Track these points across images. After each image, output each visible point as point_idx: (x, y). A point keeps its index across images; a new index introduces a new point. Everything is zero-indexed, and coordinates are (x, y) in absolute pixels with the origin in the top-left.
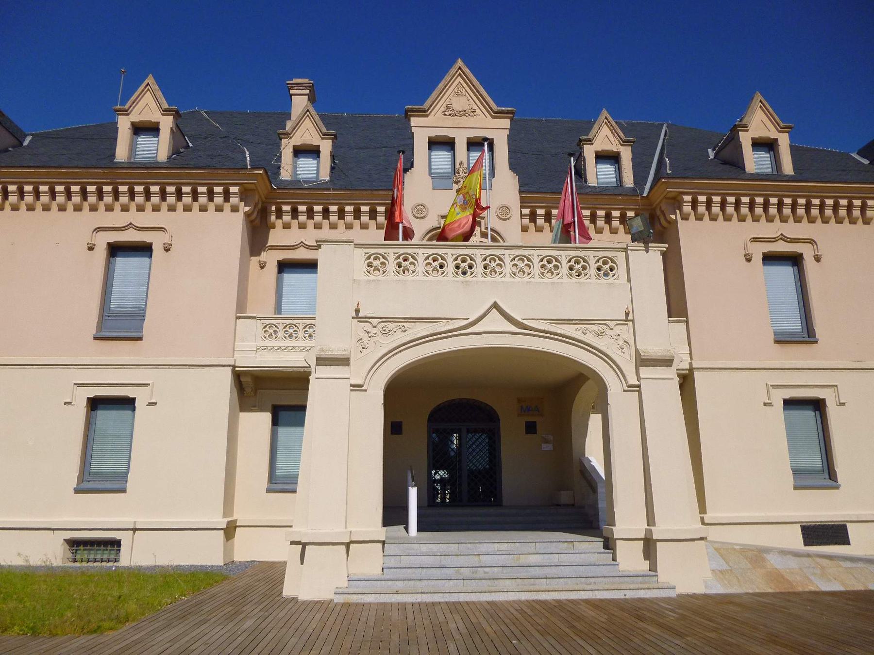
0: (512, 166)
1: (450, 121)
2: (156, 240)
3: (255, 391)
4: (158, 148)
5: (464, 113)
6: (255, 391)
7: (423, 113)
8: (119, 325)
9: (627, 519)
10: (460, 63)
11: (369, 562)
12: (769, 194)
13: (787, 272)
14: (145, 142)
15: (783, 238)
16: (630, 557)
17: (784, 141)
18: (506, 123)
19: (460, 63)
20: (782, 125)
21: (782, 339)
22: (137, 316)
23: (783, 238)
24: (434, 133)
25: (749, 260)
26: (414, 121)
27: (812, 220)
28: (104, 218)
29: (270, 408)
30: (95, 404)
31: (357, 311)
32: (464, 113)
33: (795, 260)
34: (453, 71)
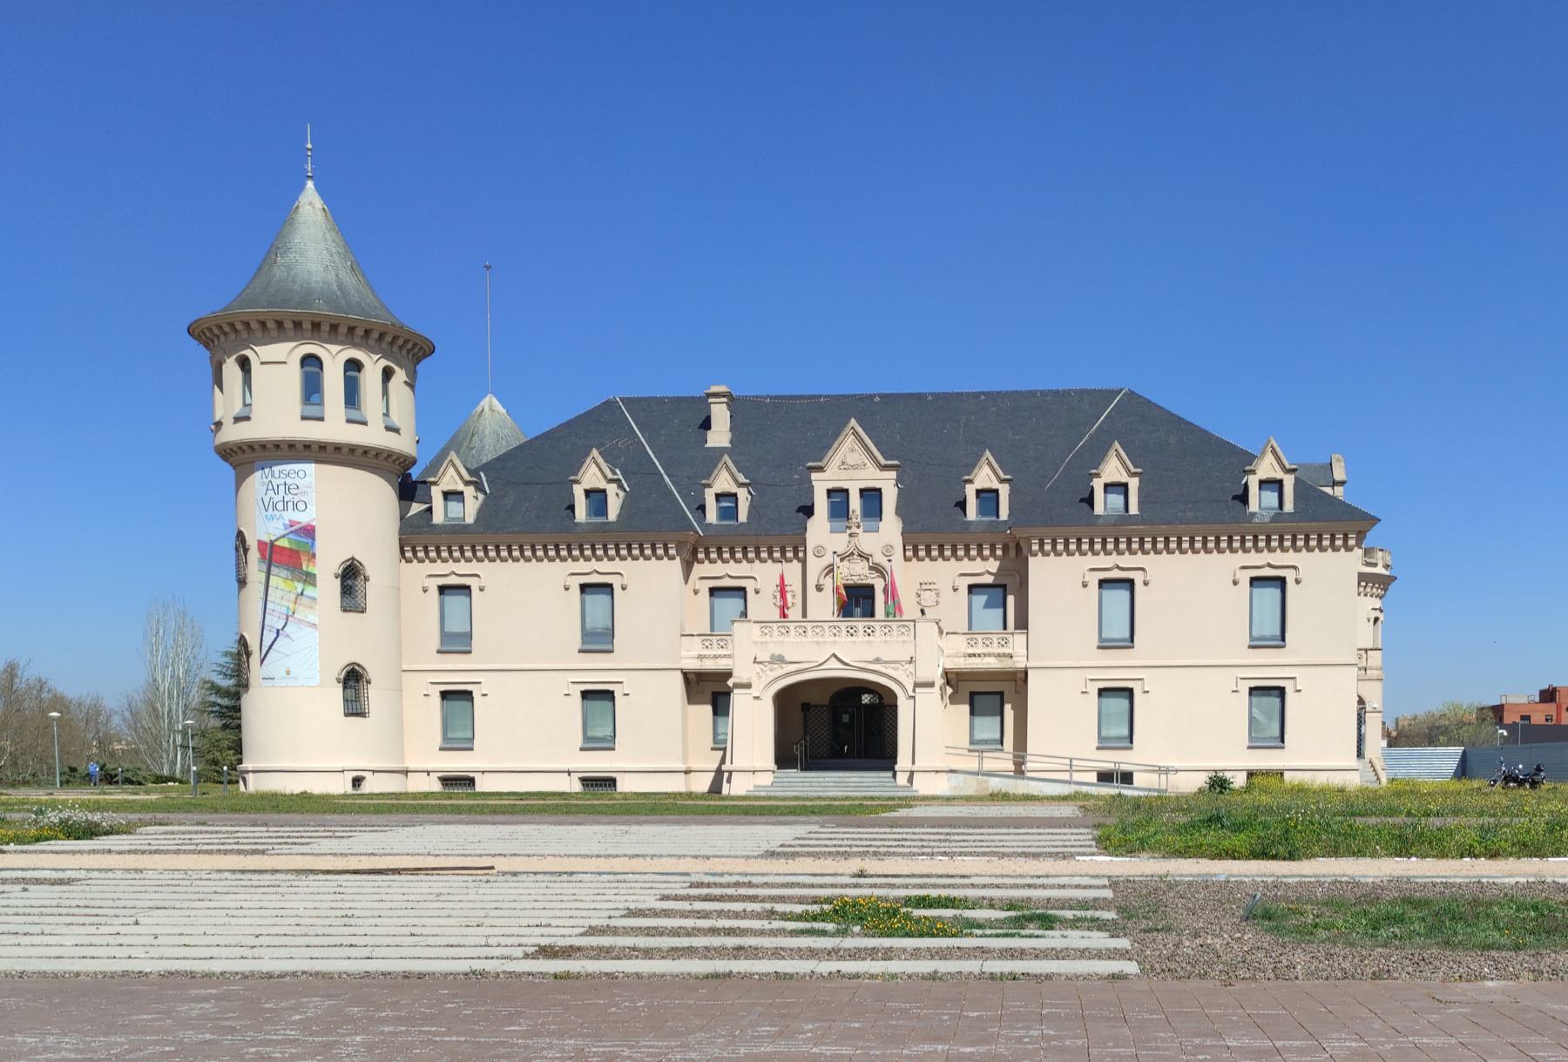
0: (899, 511)
1: (844, 474)
2: (615, 581)
3: (698, 682)
4: (470, 507)
5: (855, 467)
6: (698, 682)
7: (821, 469)
8: (598, 639)
9: (903, 761)
10: (853, 422)
11: (766, 780)
12: (1122, 532)
13: (1273, 593)
14: (454, 506)
15: (1270, 565)
16: (902, 779)
17: (1134, 484)
18: (893, 474)
19: (853, 422)
20: (610, 476)
21: (1105, 645)
22: (610, 633)
23: (1270, 565)
24: (831, 485)
25: (567, 589)
26: (814, 476)
27: (1145, 553)
28: (440, 568)
29: (709, 696)
30: (1102, 692)
31: (682, 627)
32: (855, 467)
33: (1281, 582)
34: (847, 430)
